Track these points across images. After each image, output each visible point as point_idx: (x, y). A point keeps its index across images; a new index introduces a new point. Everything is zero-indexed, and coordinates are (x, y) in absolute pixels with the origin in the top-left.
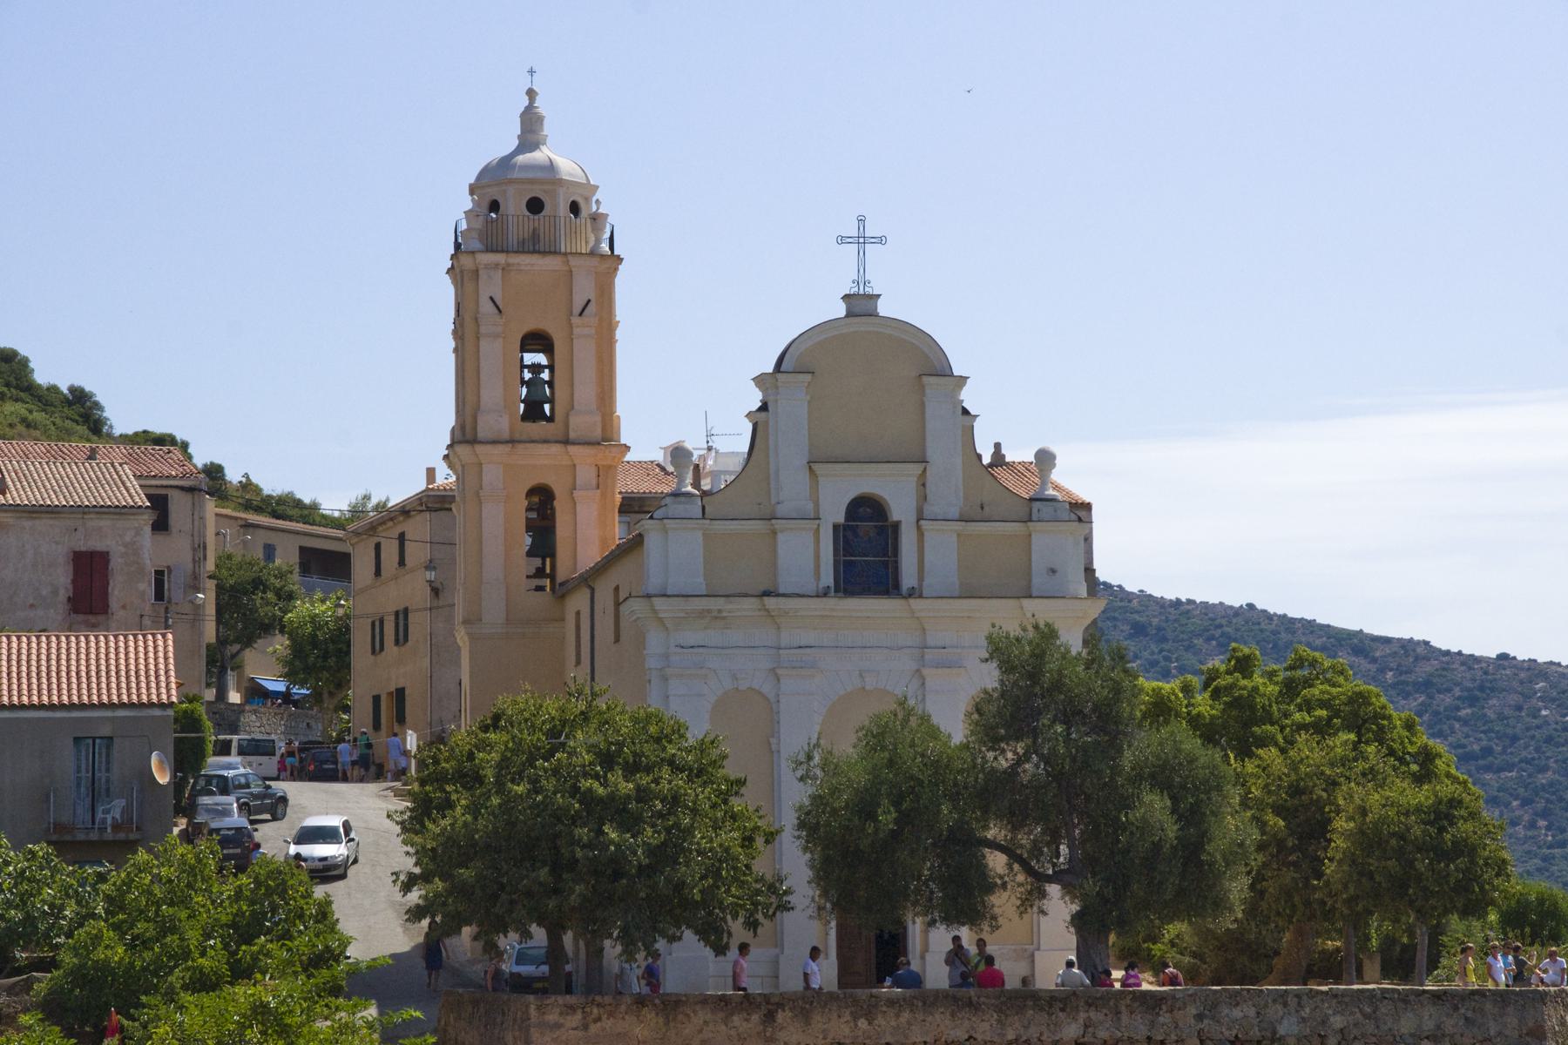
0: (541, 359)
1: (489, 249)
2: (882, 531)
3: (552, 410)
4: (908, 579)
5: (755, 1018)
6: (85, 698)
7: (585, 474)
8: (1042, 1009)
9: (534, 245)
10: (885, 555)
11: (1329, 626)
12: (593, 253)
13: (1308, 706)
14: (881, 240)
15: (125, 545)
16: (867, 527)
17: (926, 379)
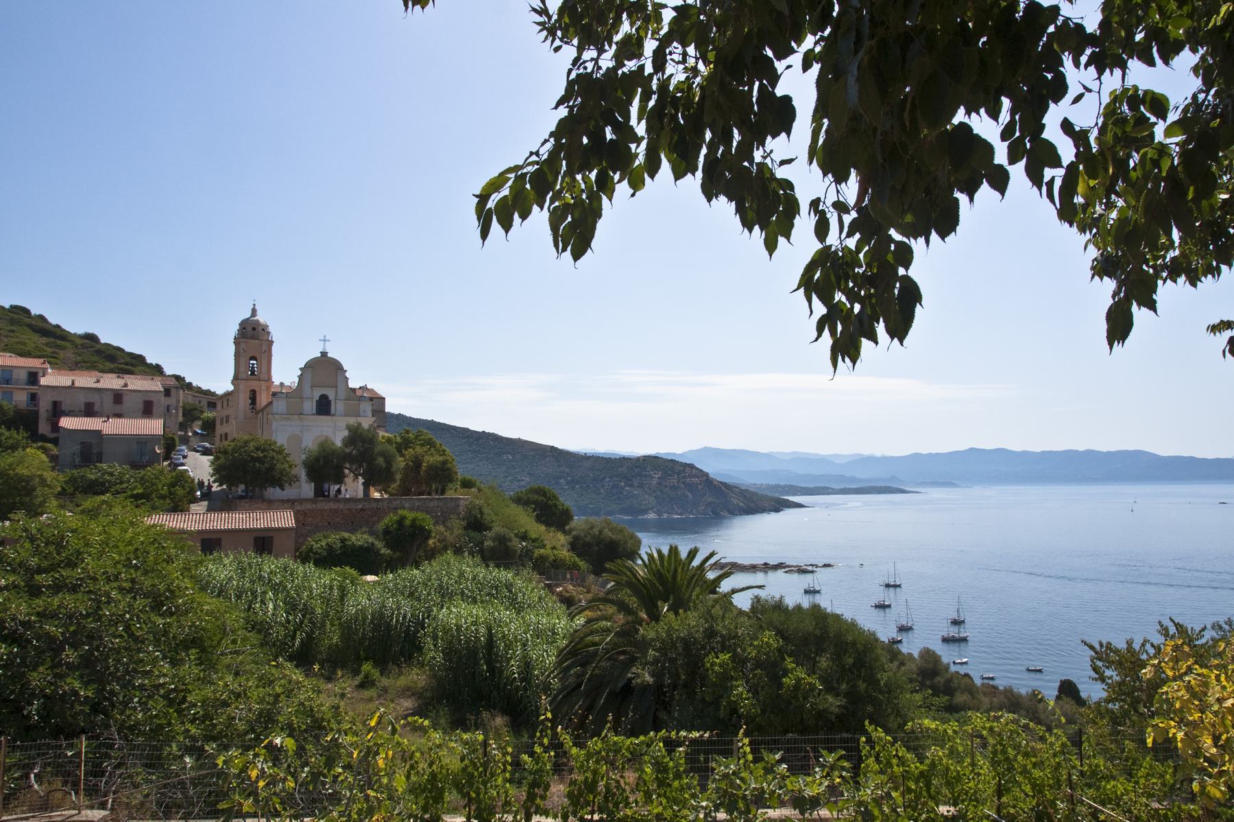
0: (255, 362)
4: (333, 412)
7: (264, 387)
9: (253, 338)
12: (268, 340)
13: (420, 440)
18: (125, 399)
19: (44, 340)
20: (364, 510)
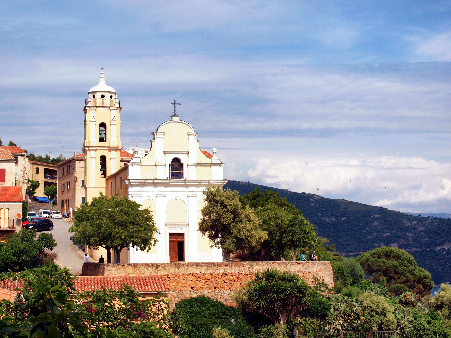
5: (154, 268)
8: (215, 266)
11: (266, 186)
16: (176, 164)
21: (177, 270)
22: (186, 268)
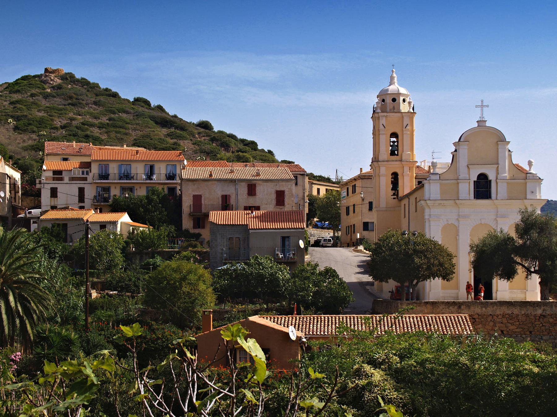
0: (395, 139)
1: (382, 112)
2: (487, 182)
3: (398, 153)
5: (456, 307)
6: (262, 227)
10: (487, 188)
14: (487, 106)
15: (288, 189)
16: (482, 181)
17: (499, 143)
18: (258, 189)
19: (165, 131)
20: (544, 316)
21: (484, 309)
22: (495, 307)
